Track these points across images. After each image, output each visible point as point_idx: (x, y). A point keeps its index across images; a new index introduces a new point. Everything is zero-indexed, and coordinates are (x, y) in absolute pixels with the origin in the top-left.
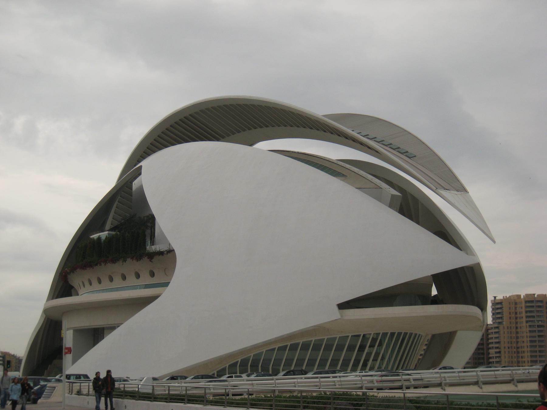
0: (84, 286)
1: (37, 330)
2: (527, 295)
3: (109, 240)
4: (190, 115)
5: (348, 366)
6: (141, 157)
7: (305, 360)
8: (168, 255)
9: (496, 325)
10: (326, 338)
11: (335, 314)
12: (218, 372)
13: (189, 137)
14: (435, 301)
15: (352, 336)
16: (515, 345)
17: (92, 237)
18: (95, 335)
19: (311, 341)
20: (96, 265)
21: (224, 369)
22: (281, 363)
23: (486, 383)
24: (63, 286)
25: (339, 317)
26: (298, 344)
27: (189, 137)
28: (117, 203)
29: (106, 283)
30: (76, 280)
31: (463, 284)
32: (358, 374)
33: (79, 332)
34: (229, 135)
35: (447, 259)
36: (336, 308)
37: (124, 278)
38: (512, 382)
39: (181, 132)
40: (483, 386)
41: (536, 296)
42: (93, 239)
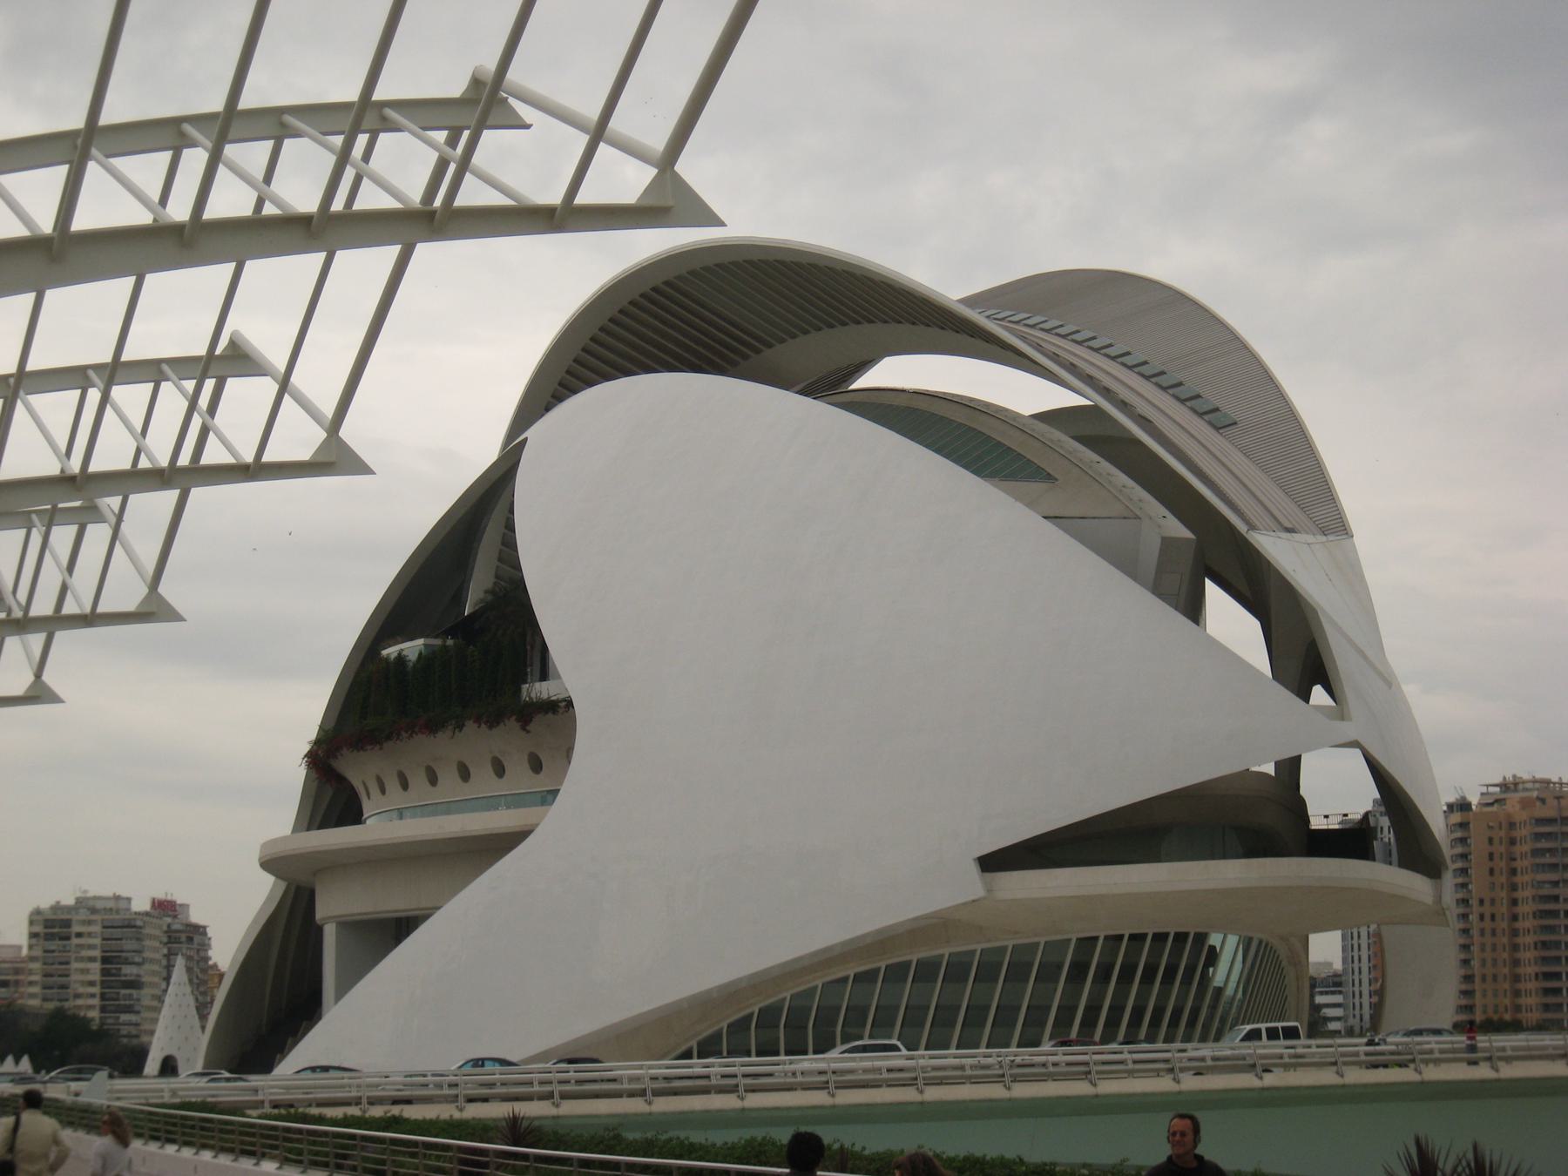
0: (383, 791)
1: (263, 922)
3: (426, 660)
4: (667, 283)
5: (1043, 1024)
6: (553, 396)
7: (1049, 1008)
8: (562, 708)
11: (970, 886)
12: (699, 1044)
15: (1106, 938)
17: (385, 652)
19: (942, 956)
20: (389, 738)
21: (716, 1037)
22: (1016, 1020)
24: (331, 793)
25: (979, 892)
26: (907, 964)
29: (449, 781)
30: (358, 770)
32: (866, 1042)
36: (974, 869)
37: (465, 774)
38: (1412, 1066)
39: (656, 317)
42: (387, 659)
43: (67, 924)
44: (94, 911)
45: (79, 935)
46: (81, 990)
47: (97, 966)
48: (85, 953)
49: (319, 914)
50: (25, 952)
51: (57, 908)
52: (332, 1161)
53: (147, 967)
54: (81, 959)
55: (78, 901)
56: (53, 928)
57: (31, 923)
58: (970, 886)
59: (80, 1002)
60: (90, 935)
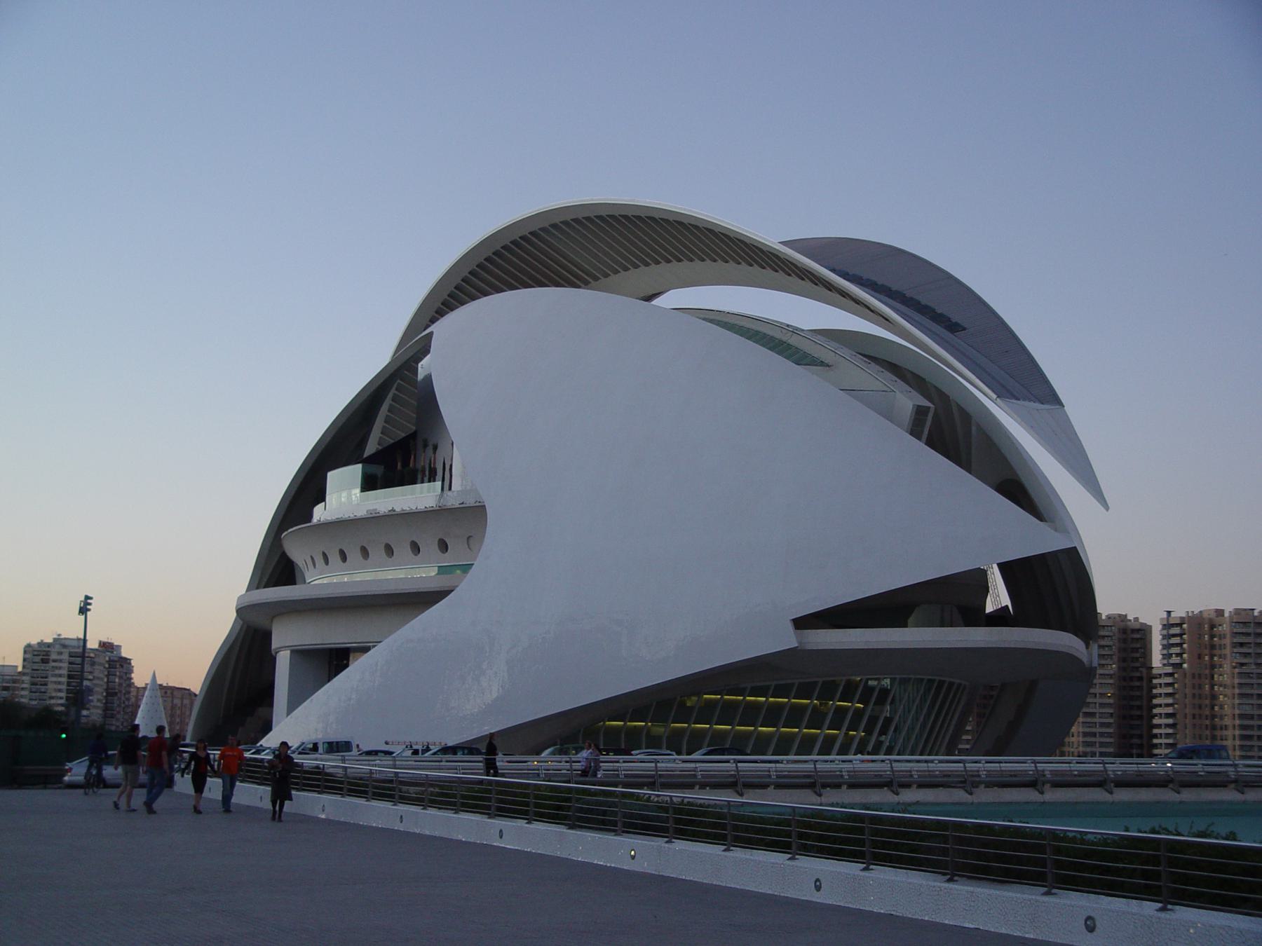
0: (327, 563)
1: (226, 649)
2: (1238, 612)
9: (1169, 670)
10: (797, 682)
13: (531, 277)
14: (1000, 619)
16: (1207, 712)
18: (335, 660)
23: (1057, 785)
25: (793, 643)
27: (531, 277)
28: (393, 391)
31: (1053, 585)
33: (301, 654)
34: (596, 279)
35: (1028, 539)
36: (790, 626)
40: (1115, 790)
41: (1256, 613)
43: (47, 654)
44: (64, 646)
45: (54, 661)
46: (54, 694)
47: (64, 680)
48: (57, 672)
49: (275, 644)
50: (20, 669)
51: (41, 644)
52: (532, 808)
53: (96, 682)
54: (56, 675)
55: (55, 640)
56: (38, 655)
57: (25, 652)
58: (787, 639)
59: (53, 702)
60: (61, 661)
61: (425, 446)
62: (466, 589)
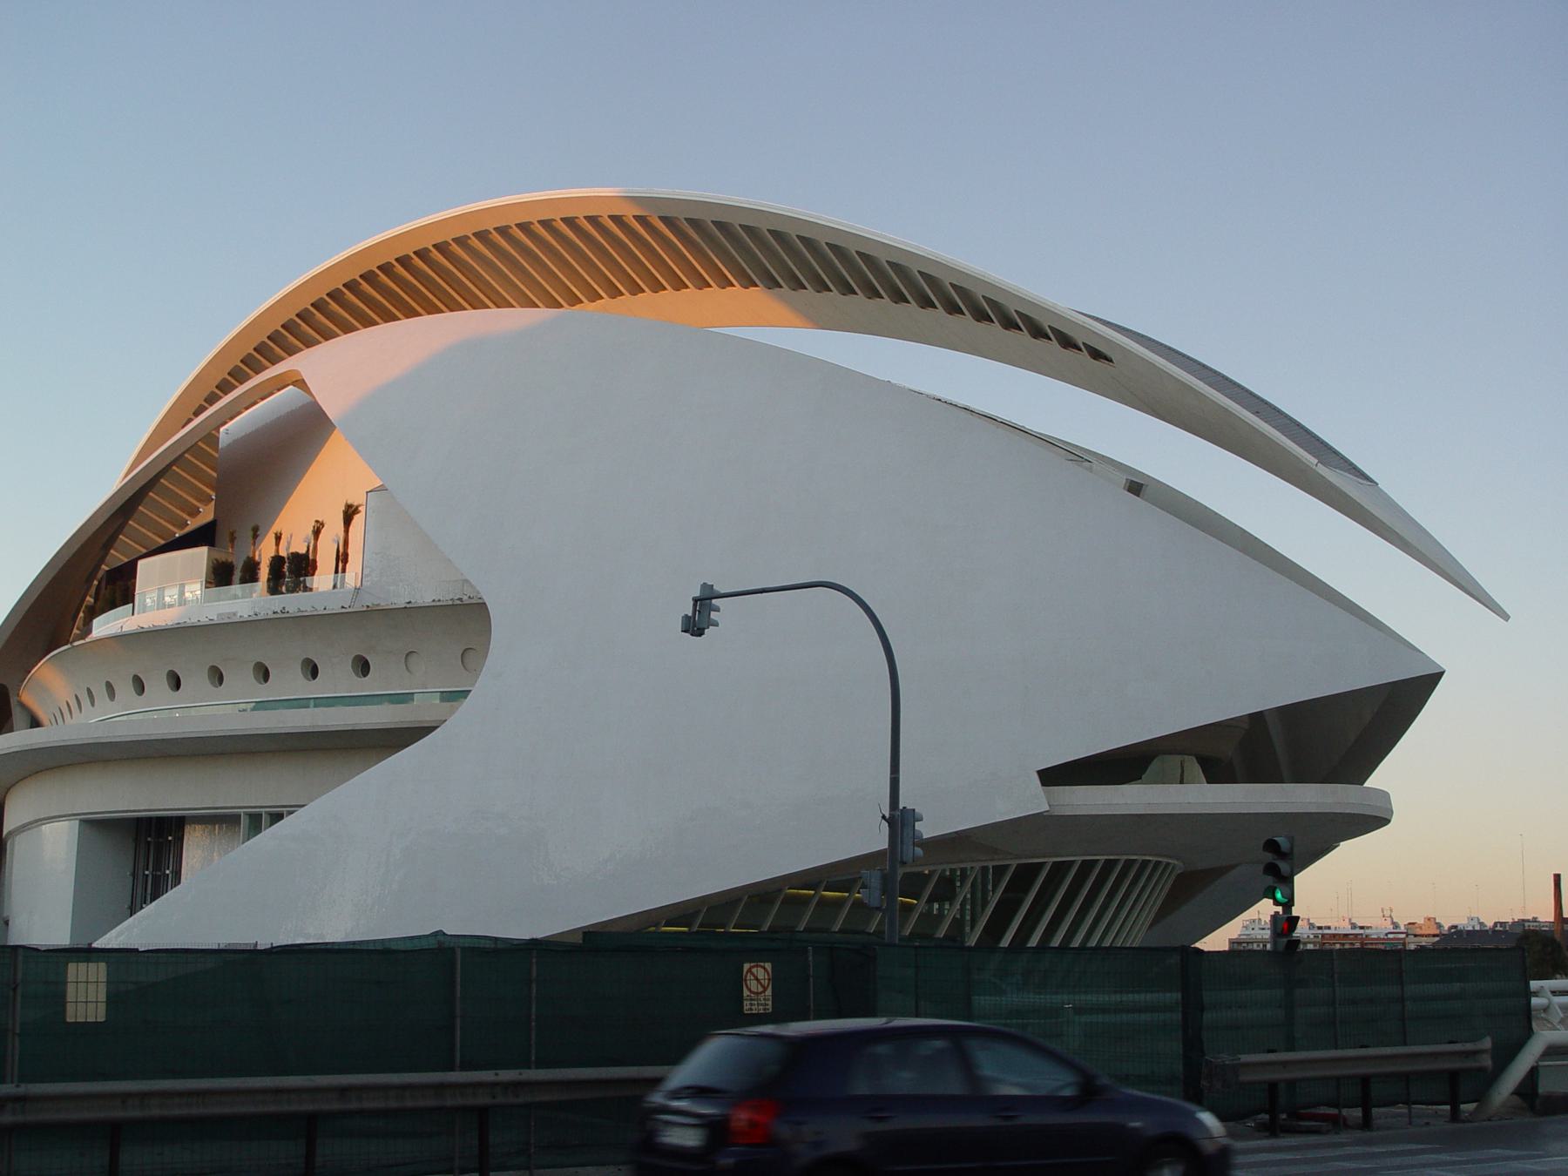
58: (1033, 800)
61: (256, 534)
62: (461, 718)
